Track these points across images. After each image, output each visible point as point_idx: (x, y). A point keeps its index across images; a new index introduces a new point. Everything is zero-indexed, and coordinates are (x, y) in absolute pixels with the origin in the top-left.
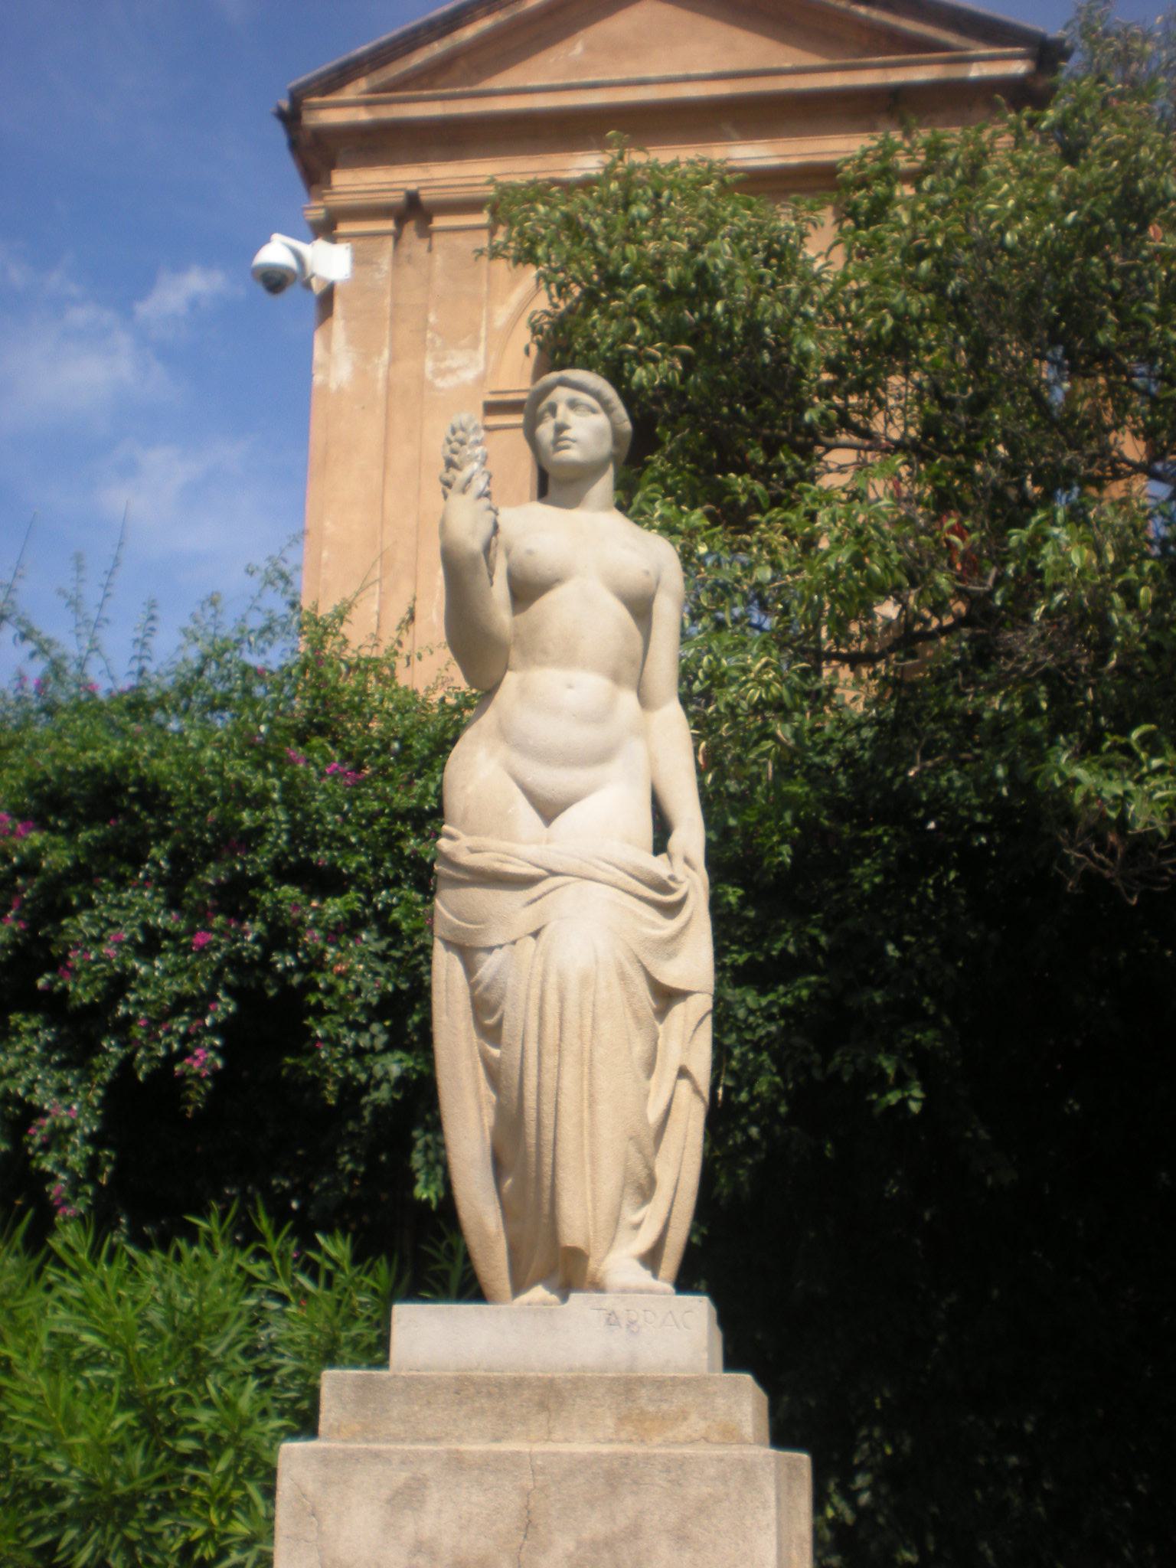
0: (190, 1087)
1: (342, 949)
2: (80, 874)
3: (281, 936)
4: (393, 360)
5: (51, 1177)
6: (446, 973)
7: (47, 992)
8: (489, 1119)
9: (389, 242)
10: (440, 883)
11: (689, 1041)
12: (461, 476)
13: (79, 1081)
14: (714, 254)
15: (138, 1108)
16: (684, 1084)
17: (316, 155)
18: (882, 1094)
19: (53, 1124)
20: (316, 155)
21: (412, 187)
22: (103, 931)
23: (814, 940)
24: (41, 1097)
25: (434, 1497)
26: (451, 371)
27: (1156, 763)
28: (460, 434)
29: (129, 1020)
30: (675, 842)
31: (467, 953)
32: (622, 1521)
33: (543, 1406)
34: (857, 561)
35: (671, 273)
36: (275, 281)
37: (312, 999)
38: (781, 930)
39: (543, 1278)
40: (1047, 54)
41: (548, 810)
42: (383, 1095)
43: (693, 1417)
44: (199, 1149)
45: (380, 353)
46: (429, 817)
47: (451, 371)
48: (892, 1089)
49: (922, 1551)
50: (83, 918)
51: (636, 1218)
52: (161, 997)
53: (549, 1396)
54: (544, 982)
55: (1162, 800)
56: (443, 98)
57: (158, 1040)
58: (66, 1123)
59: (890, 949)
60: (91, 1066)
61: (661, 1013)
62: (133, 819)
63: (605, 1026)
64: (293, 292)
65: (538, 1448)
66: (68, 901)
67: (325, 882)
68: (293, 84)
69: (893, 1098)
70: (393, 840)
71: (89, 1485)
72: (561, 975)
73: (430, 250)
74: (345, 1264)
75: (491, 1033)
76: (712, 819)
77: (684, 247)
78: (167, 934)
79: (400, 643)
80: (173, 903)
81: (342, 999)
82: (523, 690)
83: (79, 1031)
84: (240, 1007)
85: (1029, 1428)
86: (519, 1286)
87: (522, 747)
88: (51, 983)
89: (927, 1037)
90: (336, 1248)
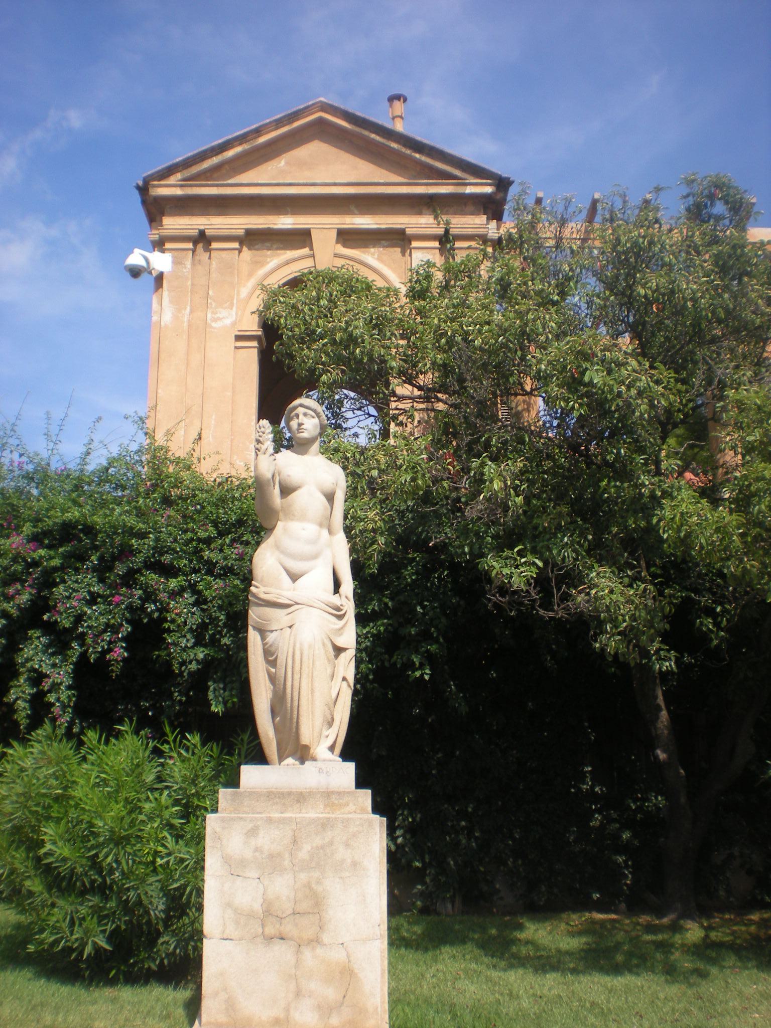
0: (113, 665)
1: (177, 603)
2: (62, 568)
3: (149, 596)
4: (191, 312)
5: (53, 705)
6: (253, 637)
7: (48, 622)
8: (270, 695)
9: (190, 253)
10: (251, 604)
11: (347, 667)
12: (263, 447)
13: (62, 661)
14: (356, 327)
15: (88, 673)
16: (345, 683)
17: (155, 209)
18: (413, 672)
19: (54, 681)
20: (155, 209)
21: (202, 227)
22: (71, 594)
23: (386, 604)
24: (46, 670)
25: (262, 833)
26: (219, 319)
27: (523, 560)
28: (262, 429)
29: (83, 634)
30: (341, 589)
31: (263, 632)
32: (327, 840)
33: (298, 801)
34: (414, 479)
35: (338, 337)
36: (135, 272)
37: (166, 625)
38: (372, 600)
39: (292, 755)
40: (503, 184)
41: (294, 577)
42: (193, 666)
43: (351, 805)
44: (107, 688)
45: (186, 309)
46: (248, 579)
47: (219, 319)
48: (417, 670)
49: (423, 862)
50: (61, 587)
51: (327, 733)
52: (99, 624)
53: (300, 798)
54: (294, 646)
55: (524, 576)
56: (217, 186)
57: (99, 644)
58: (59, 681)
59: (419, 609)
60: (67, 655)
61: (337, 656)
62: (81, 541)
63: (317, 663)
64: (144, 276)
65: (298, 815)
66: (54, 580)
67: (168, 571)
68: (145, 175)
69: (418, 674)
70: (197, 552)
71: (112, 831)
72: (301, 644)
73: (210, 258)
74: (199, 746)
75: (273, 663)
76: (355, 578)
77: (343, 325)
78: (99, 596)
79: (194, 450)
80: (102, 580)
81: (179, 626)
82: (285, 530)
83: (60, 640)
84: (133, 629)
85: (470, 810)
86: (281, 759)
87: (283, 552)
88: (49, 618)
89: (433, 648)
90: (194, 739)
